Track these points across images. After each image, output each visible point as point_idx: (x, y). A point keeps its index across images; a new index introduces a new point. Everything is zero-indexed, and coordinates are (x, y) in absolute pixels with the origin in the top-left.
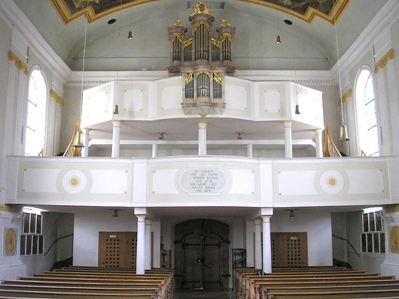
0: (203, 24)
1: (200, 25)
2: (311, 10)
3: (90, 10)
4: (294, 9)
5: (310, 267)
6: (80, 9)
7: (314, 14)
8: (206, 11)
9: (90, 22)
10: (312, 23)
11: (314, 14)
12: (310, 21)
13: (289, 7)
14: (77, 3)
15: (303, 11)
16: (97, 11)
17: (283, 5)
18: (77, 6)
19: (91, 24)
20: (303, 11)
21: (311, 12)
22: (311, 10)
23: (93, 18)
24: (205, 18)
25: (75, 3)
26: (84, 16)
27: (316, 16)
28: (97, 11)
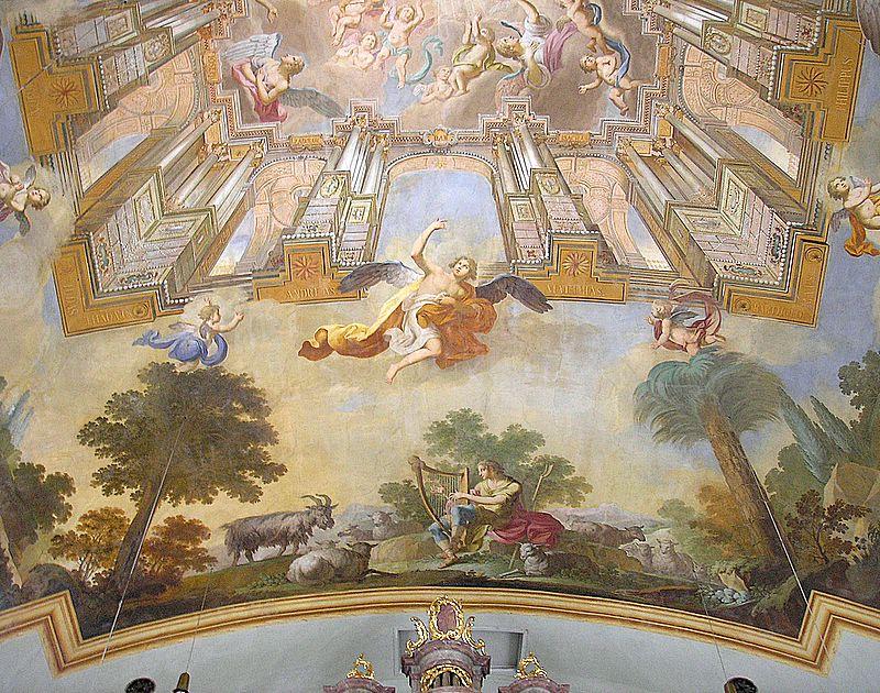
0: (452, 674)
1: (441, 675)
2: (821, 607)
3: (61, 609)
4: (760, 623)
5: (38, 623)
6: (25, 596)
7: (818, 599)
8: (460, 633)
9: (61, 670)
10: (827, 664)
11: (833, 621)
12: (817, 661)
13: (740, 615)
14: (17, 565)
15: (790, 619)
16: (93, 625)
17: (718, 612)
18: (17, 580)
19: (65, 676)
20: (790, 619)
21: (822, 614)
22: (821, 607)
23: (73, 651)
24: (457, 656)
25: (10, 564)
26: (37, 633)
27: (840, 627)
28: (93, 625)
